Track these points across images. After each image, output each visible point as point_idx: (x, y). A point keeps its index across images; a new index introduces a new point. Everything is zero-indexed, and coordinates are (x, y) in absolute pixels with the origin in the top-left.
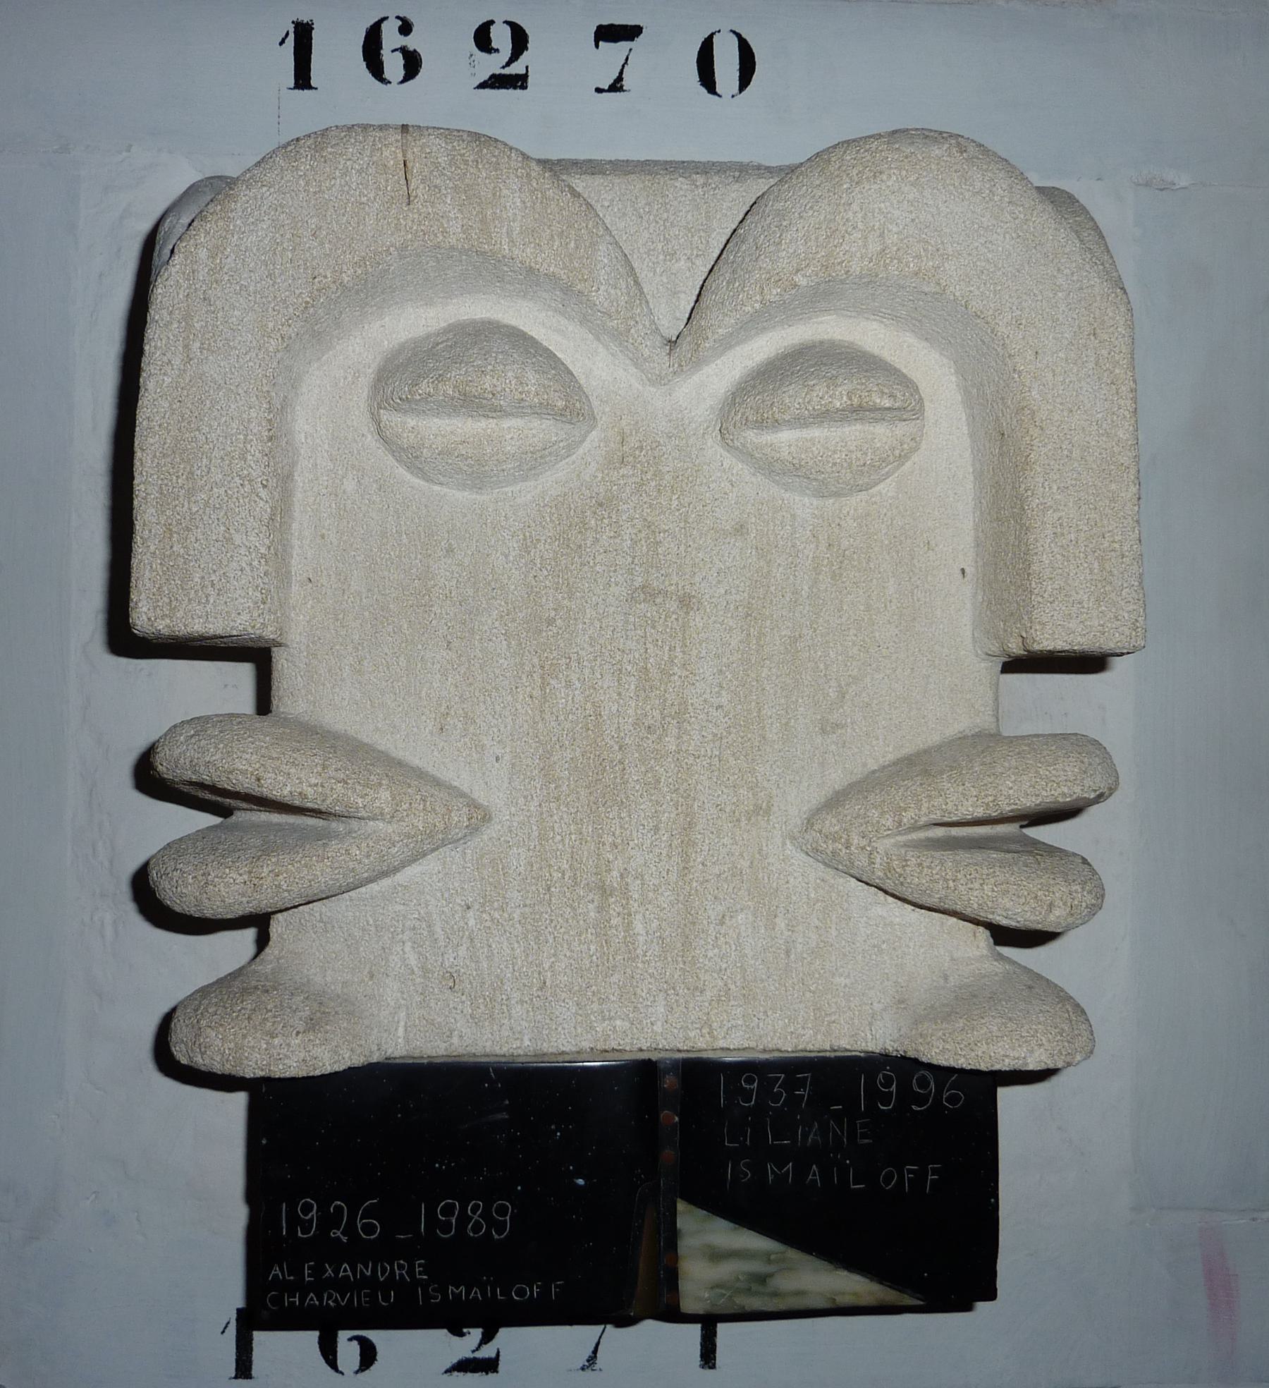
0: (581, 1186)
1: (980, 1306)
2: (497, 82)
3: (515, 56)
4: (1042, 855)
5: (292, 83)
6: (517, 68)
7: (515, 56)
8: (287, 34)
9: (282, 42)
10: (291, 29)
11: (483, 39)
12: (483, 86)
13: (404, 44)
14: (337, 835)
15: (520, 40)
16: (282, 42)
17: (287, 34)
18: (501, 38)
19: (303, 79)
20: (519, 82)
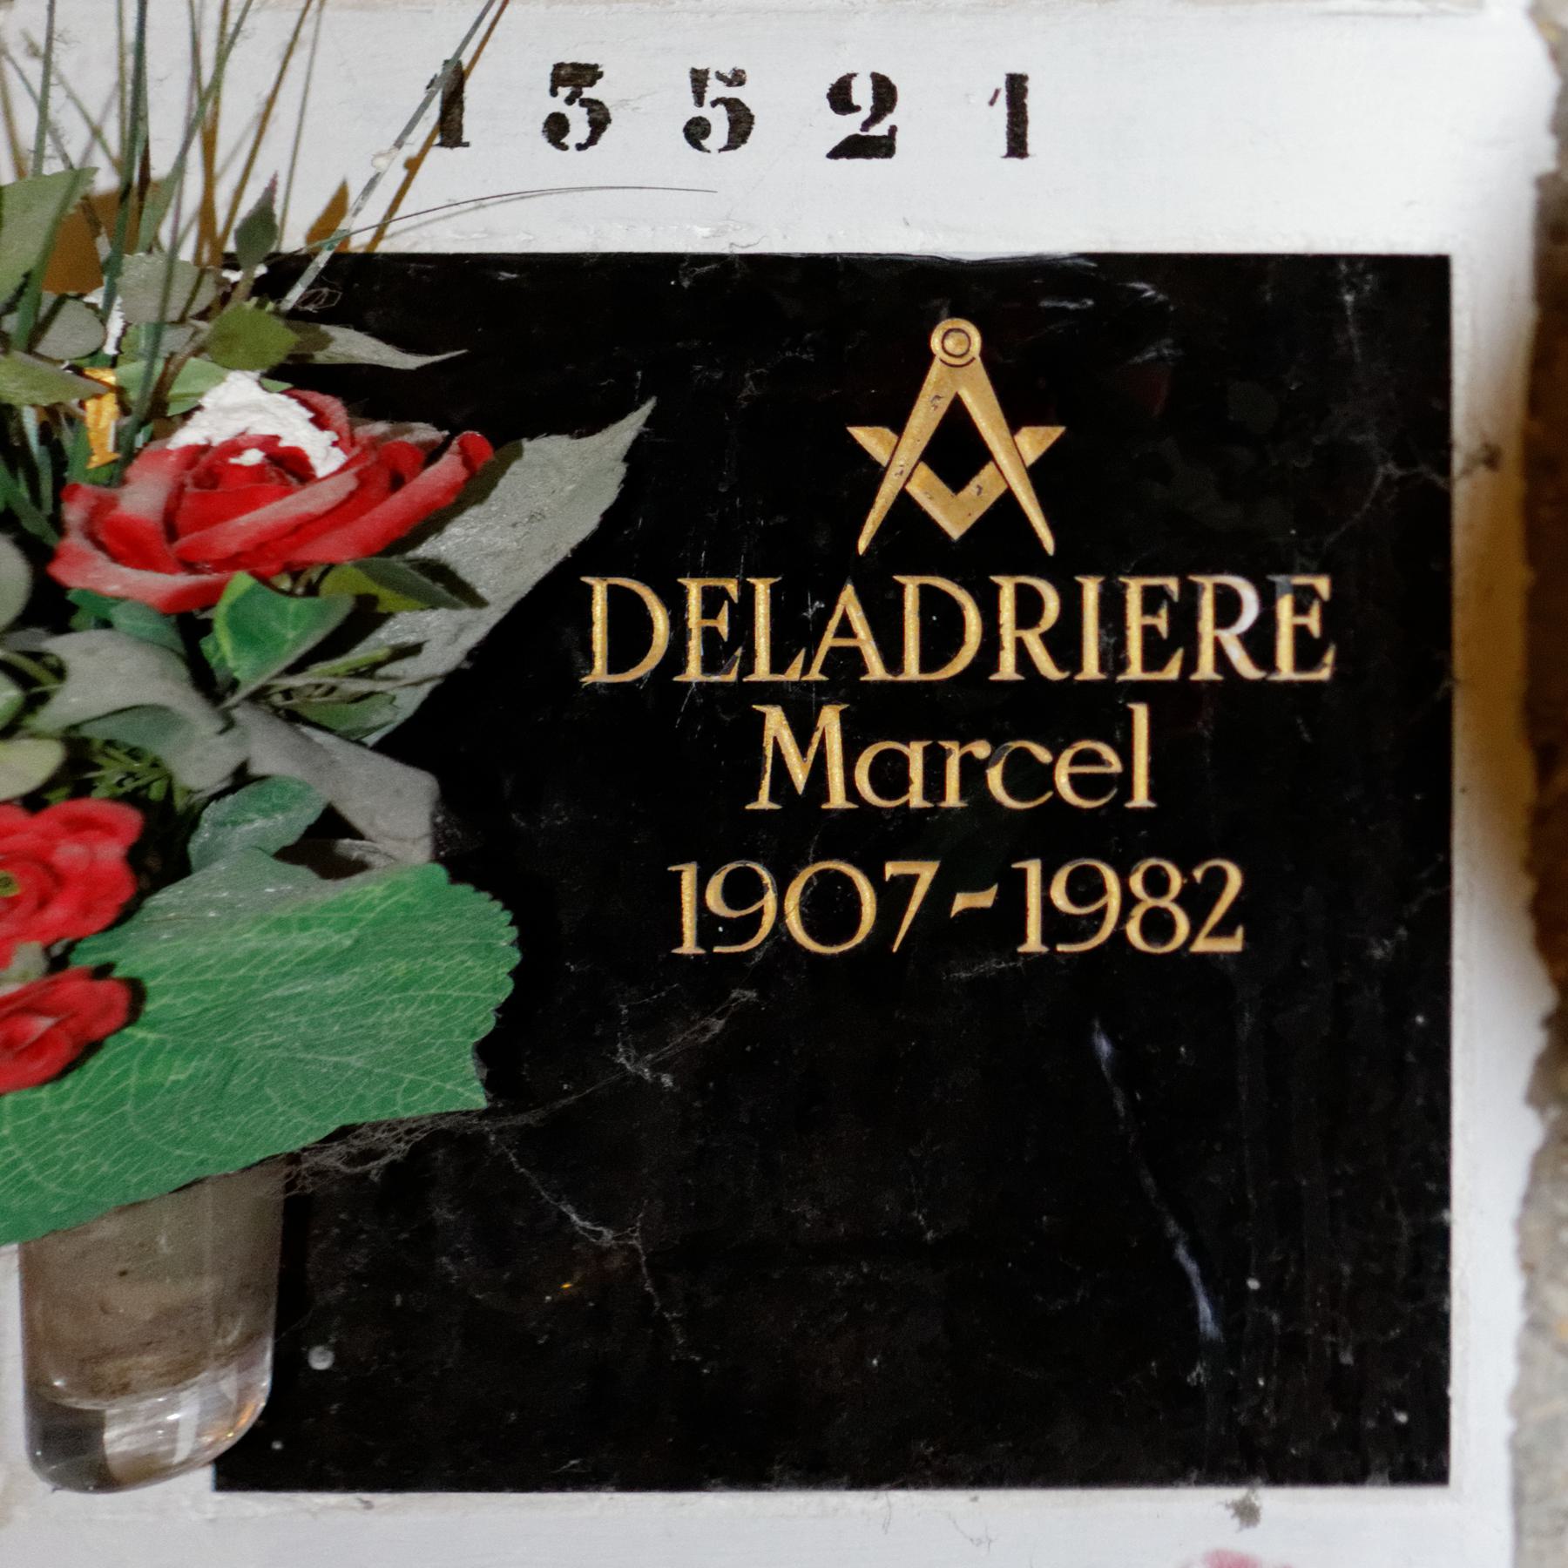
0: (1258, 1385)
1: (487, 1026)
2: (852, 148)
3: (875, 118)
4: (453, 927)
5: (1005, 151)
6: (879, 130)
7: (875, 118)
8: (997, 92)
9: (992, 103)
10: (1002, 85)
11: (840, 98)
12: (835, 154)
13: (563, 111)
14: (187, 344)
15: (885, 94)
16: (992, 103)
17: (997, 92)
18: (862, 94)
19: (1017, 146)
20: (883, 147)
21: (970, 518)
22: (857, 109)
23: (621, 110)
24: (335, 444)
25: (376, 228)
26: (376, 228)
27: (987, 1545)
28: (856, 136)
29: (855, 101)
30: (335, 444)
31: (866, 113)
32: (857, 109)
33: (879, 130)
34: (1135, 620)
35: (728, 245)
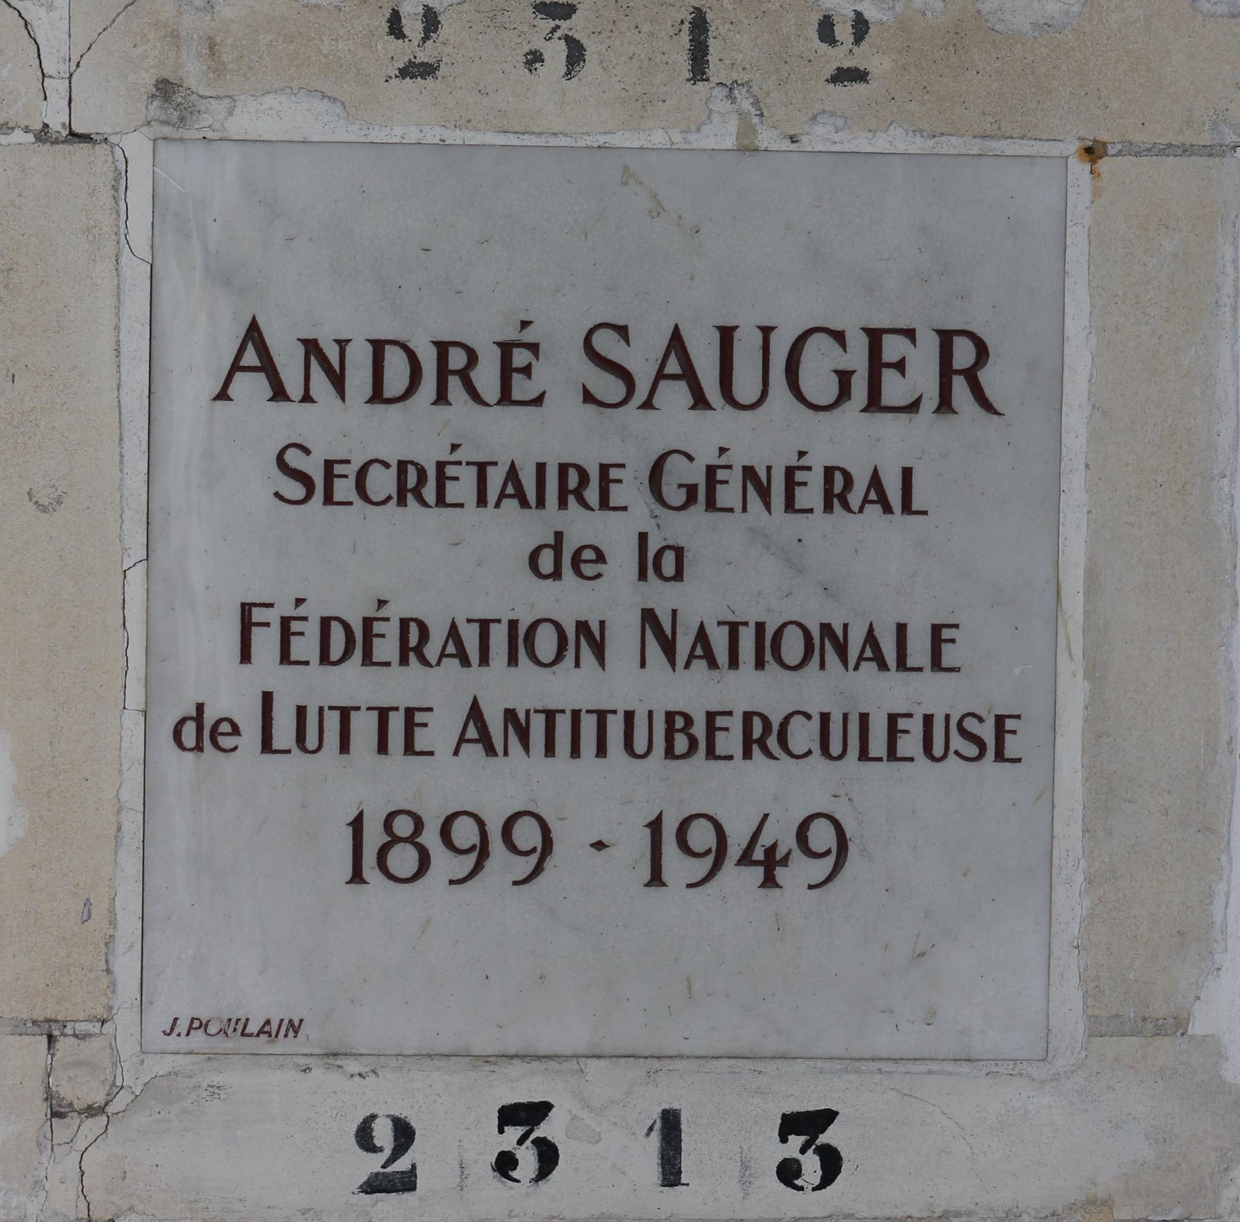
2: (374, 1186)
6: (402, 1165)
11: (364, 1137)
15: (404, 1134)
20: (407, 1182)
21: (542, 70)
22: (381, 1150)
23: (555, 33)
24: (853, 33)
25: (451, 640)
26: (451, 640)
27: (162, 118)
28: (377, 1174)
29: (378, 1143)
30: (853, 33)
31: (387, 1153)
32: (381, 1150)
33: (402, 1165)
35: (561, 41)
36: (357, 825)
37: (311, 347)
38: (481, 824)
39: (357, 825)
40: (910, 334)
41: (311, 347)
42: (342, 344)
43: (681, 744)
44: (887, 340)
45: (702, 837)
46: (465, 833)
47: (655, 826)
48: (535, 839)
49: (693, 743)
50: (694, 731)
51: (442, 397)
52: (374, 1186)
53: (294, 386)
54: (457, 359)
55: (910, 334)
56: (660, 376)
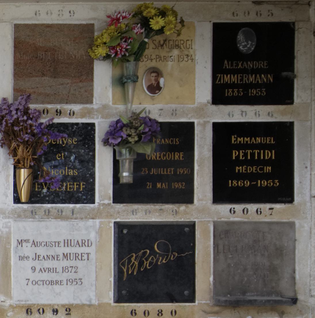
6: (69, 313)
20: (70, 314)
34: (68, 186)
36: (63, 268)
37: (47, 256)
38: (72, 279)
39: (63, 268)
40: (84, 253)
41: (47, 256)
42: (50, 255)
43: (53, 284)
44: (83, 254)
45: (71, 281)
46: (71, 281)
47: (67, 280)
48: (72, 281)
49: (54, 284)
50: (54, 282)
51: (56, 284)
52: (67, 314)
53: (46, 259)
54: (57, 282)
55: (84, 253)
56: (77, 244)
